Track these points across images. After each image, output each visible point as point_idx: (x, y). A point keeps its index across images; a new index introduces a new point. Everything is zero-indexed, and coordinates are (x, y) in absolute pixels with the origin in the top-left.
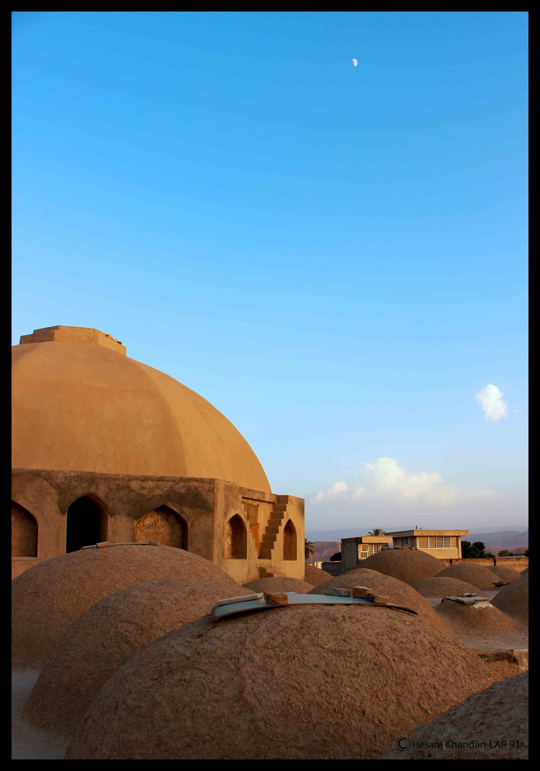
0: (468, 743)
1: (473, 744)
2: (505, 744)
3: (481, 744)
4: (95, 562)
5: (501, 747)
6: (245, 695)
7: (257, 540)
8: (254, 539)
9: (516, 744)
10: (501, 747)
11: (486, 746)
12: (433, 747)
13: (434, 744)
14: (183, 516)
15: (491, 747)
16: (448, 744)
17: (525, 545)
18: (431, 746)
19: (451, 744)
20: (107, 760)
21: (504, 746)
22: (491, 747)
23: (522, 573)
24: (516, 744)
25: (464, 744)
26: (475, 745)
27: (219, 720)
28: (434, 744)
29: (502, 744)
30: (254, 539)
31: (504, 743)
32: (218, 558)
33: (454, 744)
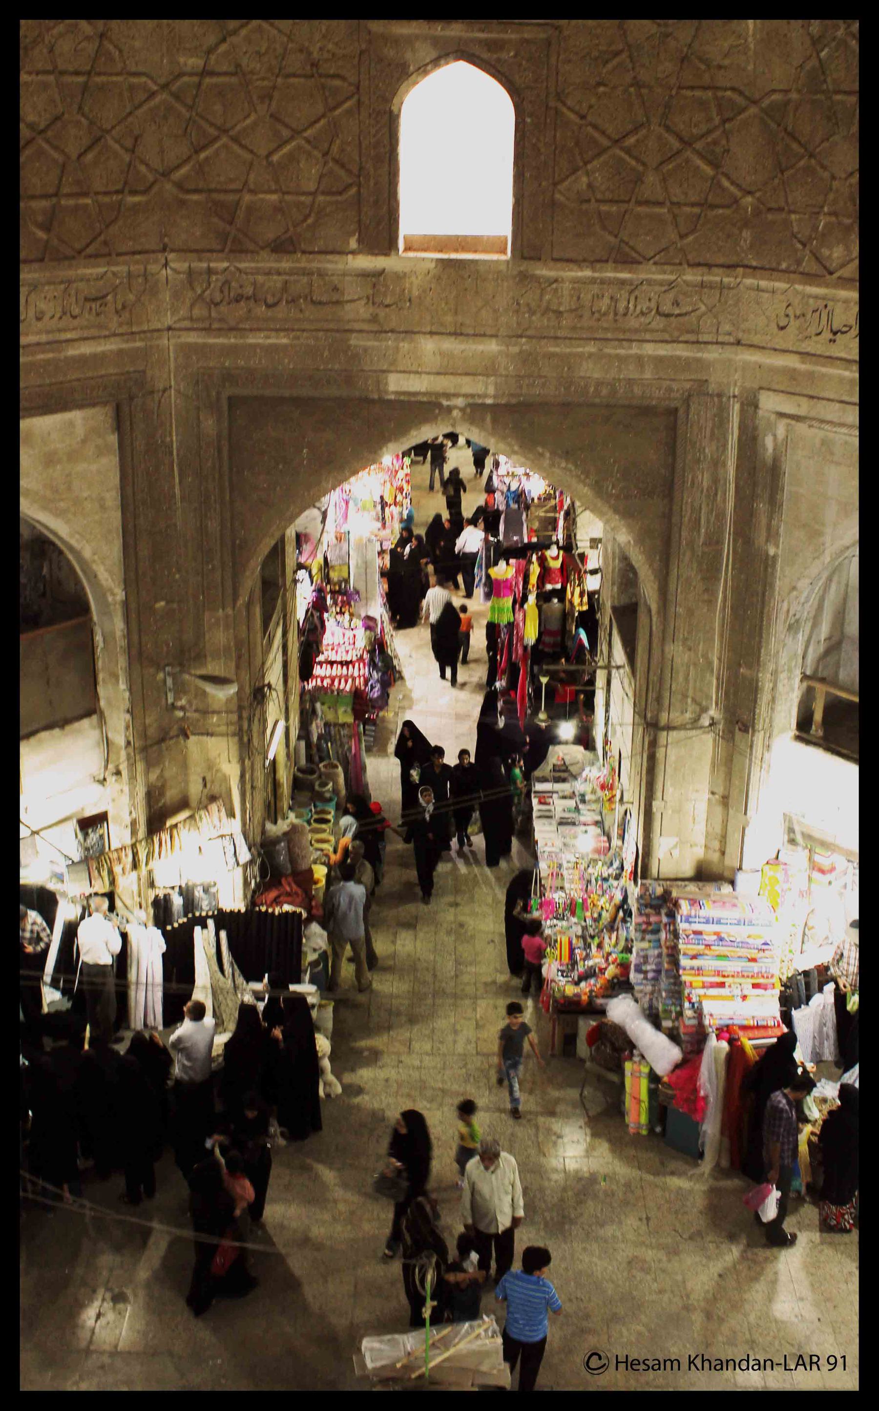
0: (737, 1362)
1: (748, 1361)
7: (242, 26)
8: (30, 949)
9: (840, 1361)
11: (782, 1362)
13: (762, 1363)
17: (22, 266)
18: (756, 1367)
19: (698, 1362)
20: (534, 1380)
21: (814, 1367)
24: (840, 1361)
25: (665, 1361)
28: (762, 1363)
29: (811, 1363)
30: (30, 949)
31: (815, 1359)
32: (692, 42)
33: (706, 1364)
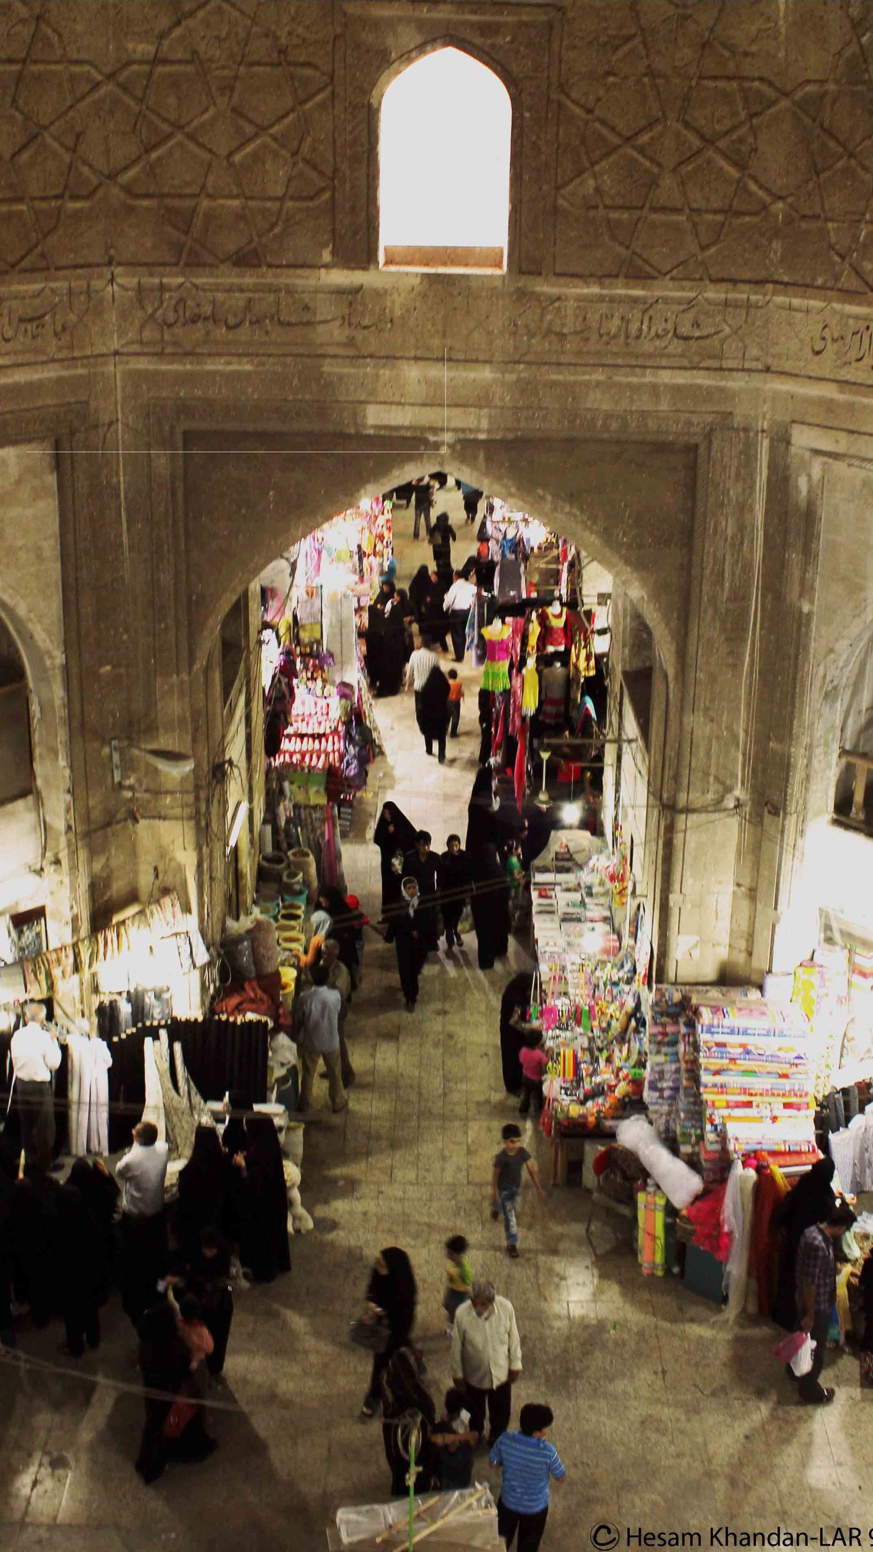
0: (766, 1536)
1: (778, 1535)
2: (856, 1537)
3: (798, 1535)
4: (389, 262)
5: (848, 1543)
6: (849, 1236)
10: (848, 1543)
12: (791, 1544)
13: (795, 1537)
14: (296, 691)
15: (822, 1544)
16: (715, 1536)
19: (722, 1536)
21: (855, 1541)
22: (822, 1544)
23: (862, 1392)
25: (755, 1535)
26: (783, 1537)
27: (744, 312)
28: (795, 1537)
29: (851, 1537)
31: (855, 1533)
